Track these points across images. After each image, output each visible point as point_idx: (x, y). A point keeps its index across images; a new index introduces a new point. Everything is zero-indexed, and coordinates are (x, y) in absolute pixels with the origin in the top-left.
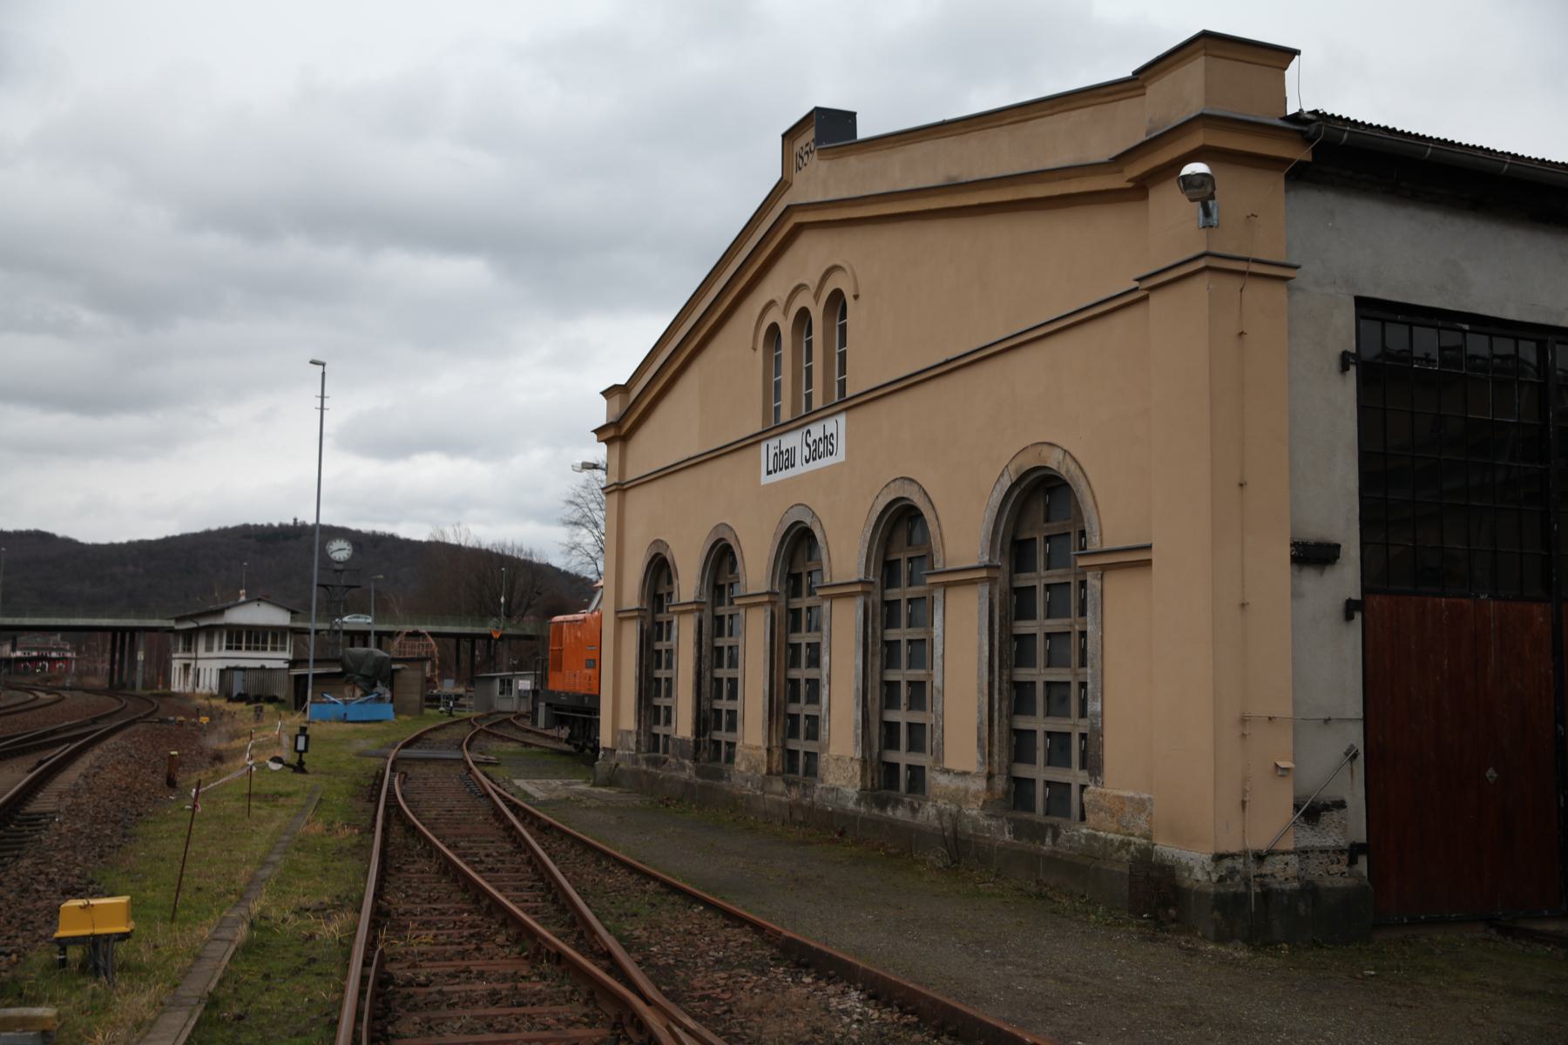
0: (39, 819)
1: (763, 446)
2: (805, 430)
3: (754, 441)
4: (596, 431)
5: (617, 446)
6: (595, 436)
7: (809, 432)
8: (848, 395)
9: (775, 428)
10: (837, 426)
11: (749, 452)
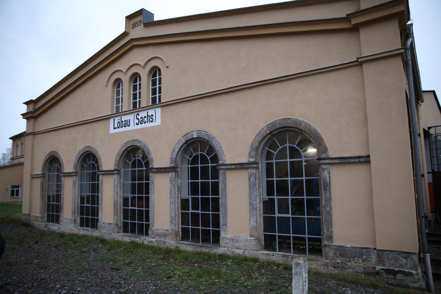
0: (178, 185)
1: (112, 121)
2: (136, 114)
3: (107, 118)
4: (22, 115)
5: (32, 121)
6: (22, 117)
7: (138, 114)
8: (162, 102)
9: (118, 113)
10: (157, 113)
11: (105, 122)
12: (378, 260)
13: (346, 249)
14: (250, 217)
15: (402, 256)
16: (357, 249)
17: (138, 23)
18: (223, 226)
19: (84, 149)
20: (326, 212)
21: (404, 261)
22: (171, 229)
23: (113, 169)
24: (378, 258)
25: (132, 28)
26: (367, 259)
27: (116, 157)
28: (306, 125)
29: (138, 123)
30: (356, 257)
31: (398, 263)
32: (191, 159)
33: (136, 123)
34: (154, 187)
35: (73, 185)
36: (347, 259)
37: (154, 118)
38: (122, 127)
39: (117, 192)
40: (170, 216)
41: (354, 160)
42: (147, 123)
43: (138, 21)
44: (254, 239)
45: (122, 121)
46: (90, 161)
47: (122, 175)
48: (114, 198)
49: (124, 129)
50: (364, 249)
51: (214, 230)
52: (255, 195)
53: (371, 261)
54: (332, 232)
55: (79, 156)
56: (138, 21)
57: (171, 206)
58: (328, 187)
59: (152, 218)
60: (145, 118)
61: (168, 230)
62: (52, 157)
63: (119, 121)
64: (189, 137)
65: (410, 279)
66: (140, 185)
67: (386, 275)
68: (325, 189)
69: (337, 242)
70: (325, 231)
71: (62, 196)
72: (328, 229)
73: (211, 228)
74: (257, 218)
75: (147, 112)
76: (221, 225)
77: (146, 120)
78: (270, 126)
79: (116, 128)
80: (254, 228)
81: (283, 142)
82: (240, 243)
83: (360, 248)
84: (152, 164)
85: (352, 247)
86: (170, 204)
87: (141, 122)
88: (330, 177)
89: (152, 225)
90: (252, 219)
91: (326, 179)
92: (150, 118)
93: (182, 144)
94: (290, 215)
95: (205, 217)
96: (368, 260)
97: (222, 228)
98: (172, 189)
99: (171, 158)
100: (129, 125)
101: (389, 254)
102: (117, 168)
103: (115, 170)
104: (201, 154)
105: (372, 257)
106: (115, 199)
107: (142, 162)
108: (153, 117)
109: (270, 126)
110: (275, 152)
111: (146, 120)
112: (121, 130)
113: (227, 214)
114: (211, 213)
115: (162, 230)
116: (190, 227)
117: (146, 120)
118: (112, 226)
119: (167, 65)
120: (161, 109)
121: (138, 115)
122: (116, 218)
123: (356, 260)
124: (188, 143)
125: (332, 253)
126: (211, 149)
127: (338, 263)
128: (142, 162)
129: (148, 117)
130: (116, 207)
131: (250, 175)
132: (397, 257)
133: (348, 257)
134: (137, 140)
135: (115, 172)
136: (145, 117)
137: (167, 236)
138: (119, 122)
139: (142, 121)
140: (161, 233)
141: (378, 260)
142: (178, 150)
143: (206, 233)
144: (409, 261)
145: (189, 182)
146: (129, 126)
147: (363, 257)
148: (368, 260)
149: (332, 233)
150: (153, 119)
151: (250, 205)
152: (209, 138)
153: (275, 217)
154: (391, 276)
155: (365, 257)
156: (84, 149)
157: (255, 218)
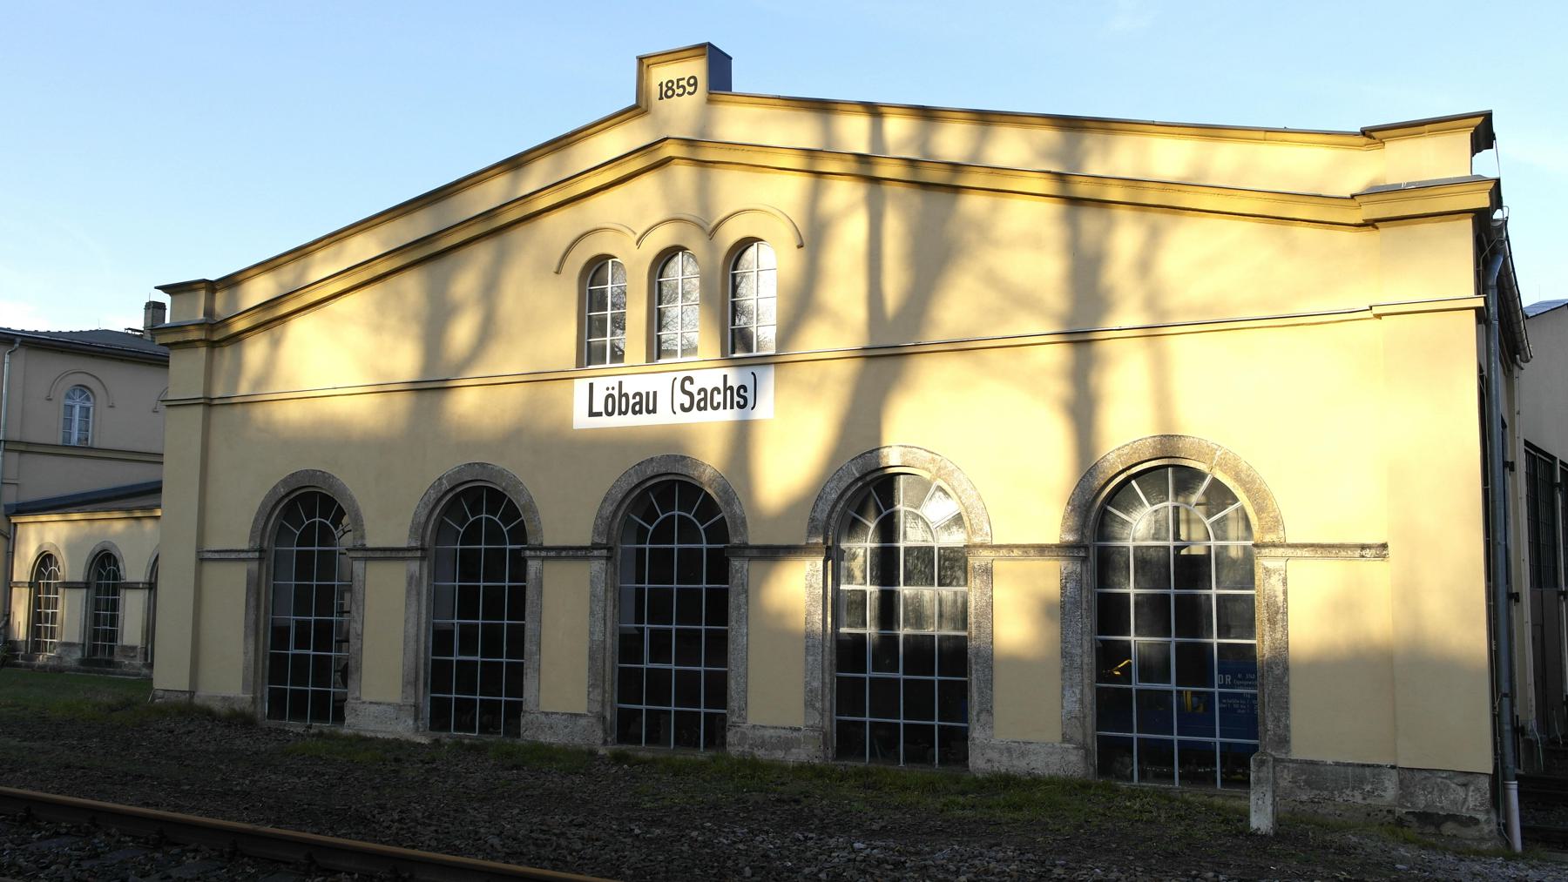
12: (1401, 792)
13: (1322, 769)
14: (1063, 689)
15: (1455, 781)
16: (1350, 768)
17: (681, 83)
18: (978, 715)
19: (461, 470)
20: (1273, 678)
21: (1461, 792)
22: (807, 726)
23: (588, 543)
24: (1401, 789)
25: (661, 98)
26: (1373, 792)
27: (601, 507)
28: (1228, 456)
29: (687, 405)
30: (1347, 788)
31: (1446, 798)
32: (462, 531)
33: (682, 405)
34: (747, 601)
35: (408, 592)
36: (1326, 793)
37: (750, 395)
38: (610, 414)
39: (605, 615)
40: (806, 688)
41: (538, 553)
42: (725, 408)
43: (684, 79)
44: (1074, 748)
45: (626, 395)
46: (310, 515)
47: (618, 563)
48: (591, 633)
49: (630, 420)
50: (1367, 769)
51: (1230, 744)
52: (1080, 631)
53: (1382, 796)
54: (1287, 727)
55: (433, 496)
56: (684, 79)
57: (810, 659)
58: (1279, 616)
59: (738, 693)
60: (716, 392)
61: (799, 729)
62: (298, 493)
63: (610, 391)
65: (1472, 832)
67: (1419, 827)
68: (1272, 622)
69: (1301, 749)
70: (1270, 726)
72: (1277, 719)
74: (1082, 691)
75: (591, 385)
76: (973, 713)
77: (718, 398)
78: (1126, 451)
79: (599, 414)
80: (1073, 720)
82: (1034, 758)
83: (1358, 765)
85: (1337, 764)
86: (807, 653)
87: (702, 404)
88: (1285, 593)
89: (740, 716)
90: (1068, 694)
91: (1276, 597)
93: (850, 481)
94: (900, 675)
95: (492, 671)
96: (1376, 794)
97: (978, 720)
98: (812, 609)
99: (812, 520)
100: (651, 408)
101: (1426, 778)
102: (605, 541)
103: (595, 547)
104: (320, 522)
105: (1386, 788)
106: (596, 638)
107: (699, 525)
108: (745, 391)
109: (1126, 451)
111: (718, 398)
113: (992, 680)
114: (504, 660)
115: (777, 731)
116: (478, 697)
118: (583, 722)
120: (204, 410)
121: (687, 383)
122: (600, 698)
123: (1348, 795)
124: (868, 478)
125: (1286, 779)
126: (512, 513)
127: (1301, 802)
128: (699, 525)
129: (729, 392)
130: (600, 663)
131: (1066, 579)
132: (1445, 784)
133: (1326, 789)
135: (596, 553)
137: (793, 747)
138: (612, 396)
140: (771, 737)
141: (1401, 792)
142: (834, 496)
143: (687, 724)
144: (1470, 794)
145: (640, 592)
146: (654, 411)
147: (1364, 787)
148: (1376, 794)
149: (1289, 731)
150: (745, 399)
151: (1062, 656)
153: (1131, 690)
154: (1432, 829)
155: (1368, 788)
156: (458, 472)
157: (1078, 691)
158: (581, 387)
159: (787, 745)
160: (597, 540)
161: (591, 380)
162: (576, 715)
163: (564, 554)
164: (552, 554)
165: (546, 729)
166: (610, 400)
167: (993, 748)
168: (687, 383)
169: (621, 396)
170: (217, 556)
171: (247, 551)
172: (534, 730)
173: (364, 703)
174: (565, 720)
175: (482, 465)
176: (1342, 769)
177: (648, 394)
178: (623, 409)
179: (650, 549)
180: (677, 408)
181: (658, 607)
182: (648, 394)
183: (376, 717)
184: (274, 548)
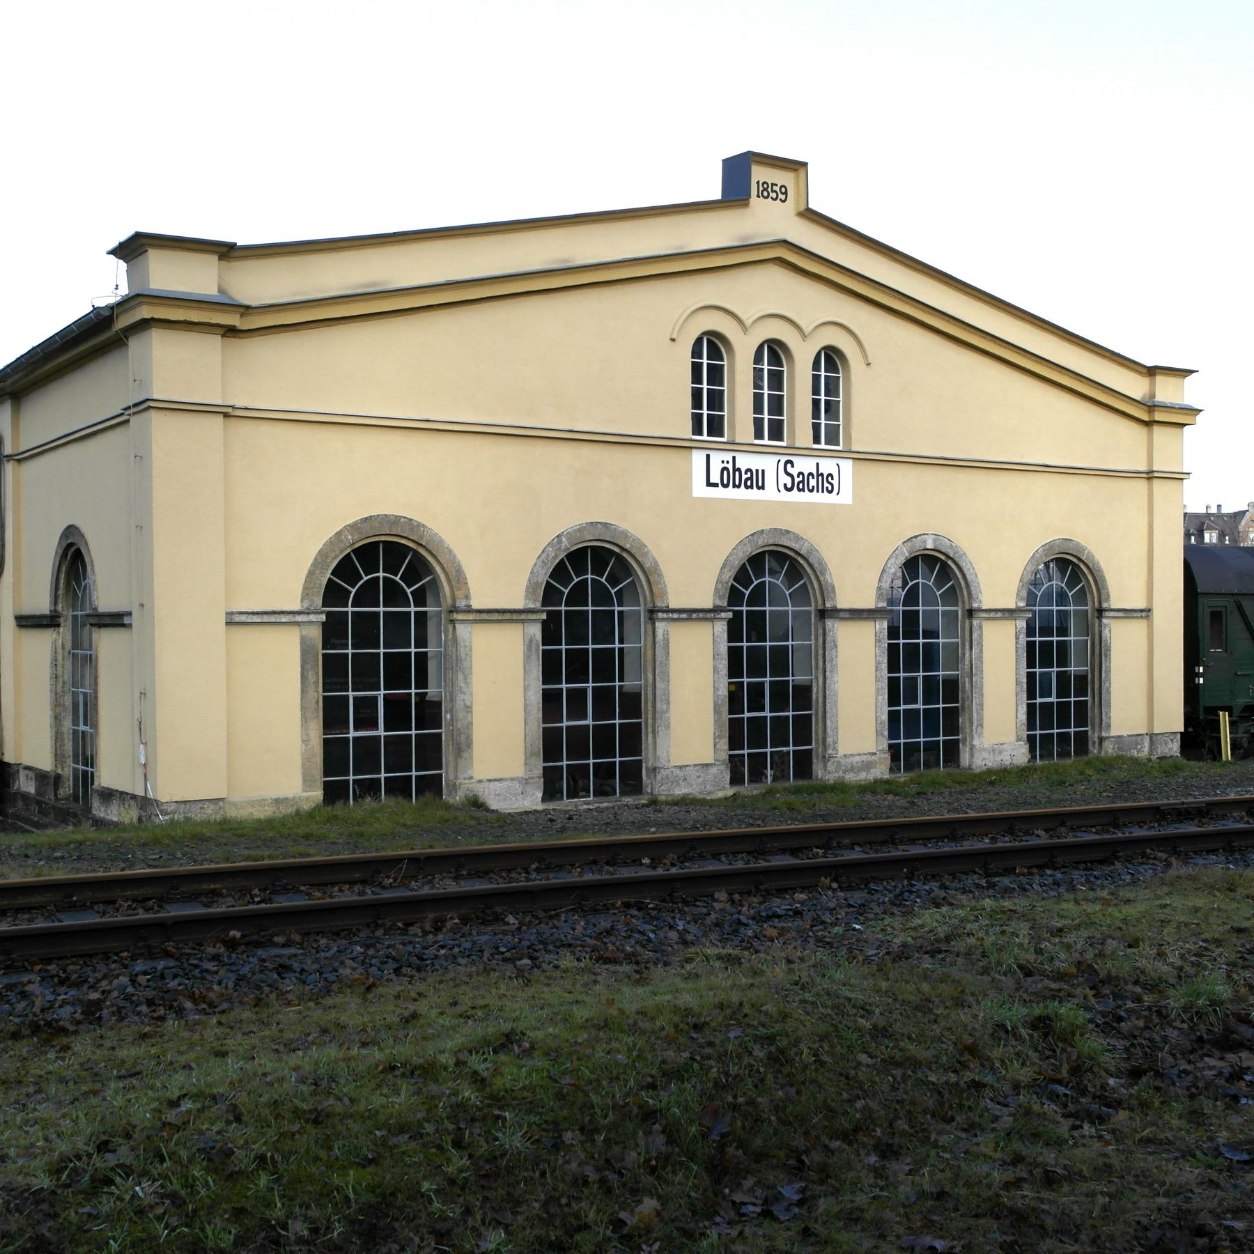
17: (775, 188)
19: (581, 529)
27: (721, 573)
29: (789, 486)
33: (785, 485)
37: (835, 482)
38: (726, 486)
45: (739, 470)
49: (742, 493)
61: (875, 754)
63: (725, 465)
64: (918, 544)
66: (1047, 647)
71: (460, 699)
73: (414, 773)
77: (813, 482)
79: (716, 485)
81: (581, 570)
84: (834, 599)
87: (749, 483)
92: (825, 483)
99: (879, 588)
103: (716, 610)
106: (720, 693)
109: (1046, 547)
110: (412, 593)
112: (731, 493)
117: (815, 485)
118: (713, 770)
119: (674, 337)
121: (789, 466)
134: (788, 532)
136: (810, 474)
139: (801, 483)
143: (605, 772)
146: (763, 487)
151: (1017, 684)
152: (955, 553)
158: (698, 458)
159: (867, 766)
160: (719, 603)
161: (708, 452)
162: (707, 765)
163: (694, 615)
164: (684, 616)
165: (681, 782)
166: (725, 472)
167: (985, 750)
168: (789, 466)
169: (735, 470)
170: (256, 619)
171: (299, 613)
172: (662, 787)
173: (480, 781)
174: (698, 771)
175: (605, 525)
176: (1133, 738)
177: (757, 471)
178: (737, 483)
179: (415, 612)
180: (781, 487)
181: (398, 670)
182: (757, 471)
183: (499, 795)
184: (71, 613)
